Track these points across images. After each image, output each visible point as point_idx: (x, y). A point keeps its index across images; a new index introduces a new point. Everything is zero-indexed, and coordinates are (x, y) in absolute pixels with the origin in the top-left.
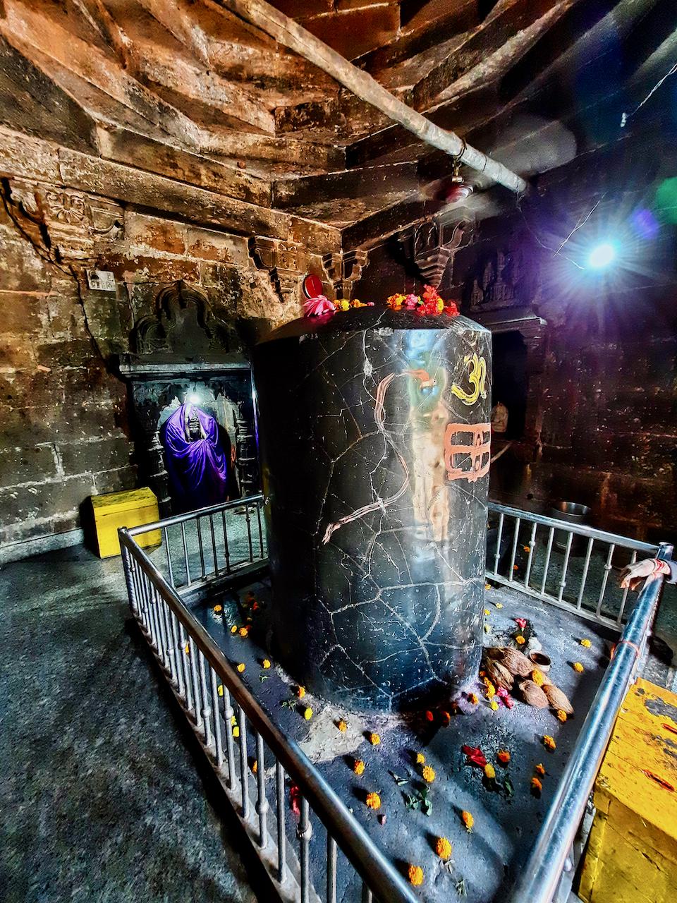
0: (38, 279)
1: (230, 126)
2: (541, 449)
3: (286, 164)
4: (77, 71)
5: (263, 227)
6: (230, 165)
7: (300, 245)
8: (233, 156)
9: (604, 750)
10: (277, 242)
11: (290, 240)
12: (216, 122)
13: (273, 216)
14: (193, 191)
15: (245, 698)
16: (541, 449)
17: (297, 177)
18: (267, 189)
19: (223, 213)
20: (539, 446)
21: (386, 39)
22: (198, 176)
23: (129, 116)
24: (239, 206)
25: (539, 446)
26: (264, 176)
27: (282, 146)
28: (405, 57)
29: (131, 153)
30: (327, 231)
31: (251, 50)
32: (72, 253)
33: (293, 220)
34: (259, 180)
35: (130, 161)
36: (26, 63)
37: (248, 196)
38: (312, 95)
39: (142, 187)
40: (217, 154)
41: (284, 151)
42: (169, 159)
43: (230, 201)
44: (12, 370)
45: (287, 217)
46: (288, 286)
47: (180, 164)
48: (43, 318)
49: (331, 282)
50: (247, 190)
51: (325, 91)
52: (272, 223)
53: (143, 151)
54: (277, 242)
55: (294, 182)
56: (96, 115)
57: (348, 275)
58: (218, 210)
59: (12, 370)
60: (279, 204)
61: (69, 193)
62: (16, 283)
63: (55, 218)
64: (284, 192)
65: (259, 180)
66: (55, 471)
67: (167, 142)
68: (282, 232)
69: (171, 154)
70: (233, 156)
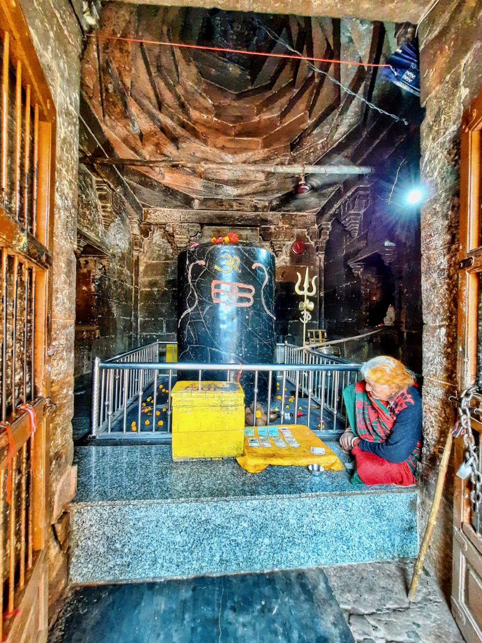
0: (170, 256)
1: (245, 183)
2: (405, 334)
3: (272, 191)
4: (184, 185)
5: (265, 221)
6: (248, 198)
7: (287, 226)
8: (247, 195)
9: (464, 636)
10: (272, 227)
11: (281, 224)
12: (239, 184)
13: (270, 215)
14: (229, 213)
15: (28, 206)
16: (405, 334)
17: (280, 195)
18: (267, 204)
19: (244, 219)
20: (404, 332)
21: (305, 126)
22: (232, 206)
23: (204, 193)
24: (252, 214)
25: (404, 332)
26: (265, 198)
27: (268, 184)
28: (312, 131)
29: (206, 205)
30: (305, 216)
31: (250, 154)
32: (182, 245)
33: (282, 215)
34: (257, 200)
35: (204, 208)
36: (169, 188)
37: (256, 209)
38: (279, 160)
39: (209, 216)
40: (240, 196)
41: (269, 186)
42: (221, 203)
43: (248, 213)
44: (156, 289)
45: (279, 214)
46: (279, 247)
47: (224, 204)
48: (169, 270)
49: (313, 243)
50: (255, 207)
51: (284, 156)
52: (269, 218)
53: (210, 203)
54: (272, 227)
55: (279, 197)
56: (194, 196)
57: (320, 238)
58: (241, 218)
59: (156, 289)
60: (273, 209)
61: (183, 224)
62: (164, 258)
63: (177, 234)
64: (274, 203)
65: (257, 200)
66: (161, 328)
67: (220, 197)
68: (275, 222)
69: (221, 201)
70: (247, 195)
